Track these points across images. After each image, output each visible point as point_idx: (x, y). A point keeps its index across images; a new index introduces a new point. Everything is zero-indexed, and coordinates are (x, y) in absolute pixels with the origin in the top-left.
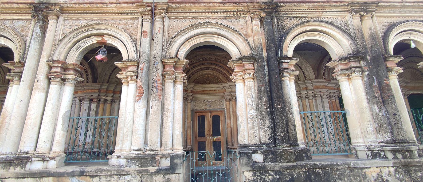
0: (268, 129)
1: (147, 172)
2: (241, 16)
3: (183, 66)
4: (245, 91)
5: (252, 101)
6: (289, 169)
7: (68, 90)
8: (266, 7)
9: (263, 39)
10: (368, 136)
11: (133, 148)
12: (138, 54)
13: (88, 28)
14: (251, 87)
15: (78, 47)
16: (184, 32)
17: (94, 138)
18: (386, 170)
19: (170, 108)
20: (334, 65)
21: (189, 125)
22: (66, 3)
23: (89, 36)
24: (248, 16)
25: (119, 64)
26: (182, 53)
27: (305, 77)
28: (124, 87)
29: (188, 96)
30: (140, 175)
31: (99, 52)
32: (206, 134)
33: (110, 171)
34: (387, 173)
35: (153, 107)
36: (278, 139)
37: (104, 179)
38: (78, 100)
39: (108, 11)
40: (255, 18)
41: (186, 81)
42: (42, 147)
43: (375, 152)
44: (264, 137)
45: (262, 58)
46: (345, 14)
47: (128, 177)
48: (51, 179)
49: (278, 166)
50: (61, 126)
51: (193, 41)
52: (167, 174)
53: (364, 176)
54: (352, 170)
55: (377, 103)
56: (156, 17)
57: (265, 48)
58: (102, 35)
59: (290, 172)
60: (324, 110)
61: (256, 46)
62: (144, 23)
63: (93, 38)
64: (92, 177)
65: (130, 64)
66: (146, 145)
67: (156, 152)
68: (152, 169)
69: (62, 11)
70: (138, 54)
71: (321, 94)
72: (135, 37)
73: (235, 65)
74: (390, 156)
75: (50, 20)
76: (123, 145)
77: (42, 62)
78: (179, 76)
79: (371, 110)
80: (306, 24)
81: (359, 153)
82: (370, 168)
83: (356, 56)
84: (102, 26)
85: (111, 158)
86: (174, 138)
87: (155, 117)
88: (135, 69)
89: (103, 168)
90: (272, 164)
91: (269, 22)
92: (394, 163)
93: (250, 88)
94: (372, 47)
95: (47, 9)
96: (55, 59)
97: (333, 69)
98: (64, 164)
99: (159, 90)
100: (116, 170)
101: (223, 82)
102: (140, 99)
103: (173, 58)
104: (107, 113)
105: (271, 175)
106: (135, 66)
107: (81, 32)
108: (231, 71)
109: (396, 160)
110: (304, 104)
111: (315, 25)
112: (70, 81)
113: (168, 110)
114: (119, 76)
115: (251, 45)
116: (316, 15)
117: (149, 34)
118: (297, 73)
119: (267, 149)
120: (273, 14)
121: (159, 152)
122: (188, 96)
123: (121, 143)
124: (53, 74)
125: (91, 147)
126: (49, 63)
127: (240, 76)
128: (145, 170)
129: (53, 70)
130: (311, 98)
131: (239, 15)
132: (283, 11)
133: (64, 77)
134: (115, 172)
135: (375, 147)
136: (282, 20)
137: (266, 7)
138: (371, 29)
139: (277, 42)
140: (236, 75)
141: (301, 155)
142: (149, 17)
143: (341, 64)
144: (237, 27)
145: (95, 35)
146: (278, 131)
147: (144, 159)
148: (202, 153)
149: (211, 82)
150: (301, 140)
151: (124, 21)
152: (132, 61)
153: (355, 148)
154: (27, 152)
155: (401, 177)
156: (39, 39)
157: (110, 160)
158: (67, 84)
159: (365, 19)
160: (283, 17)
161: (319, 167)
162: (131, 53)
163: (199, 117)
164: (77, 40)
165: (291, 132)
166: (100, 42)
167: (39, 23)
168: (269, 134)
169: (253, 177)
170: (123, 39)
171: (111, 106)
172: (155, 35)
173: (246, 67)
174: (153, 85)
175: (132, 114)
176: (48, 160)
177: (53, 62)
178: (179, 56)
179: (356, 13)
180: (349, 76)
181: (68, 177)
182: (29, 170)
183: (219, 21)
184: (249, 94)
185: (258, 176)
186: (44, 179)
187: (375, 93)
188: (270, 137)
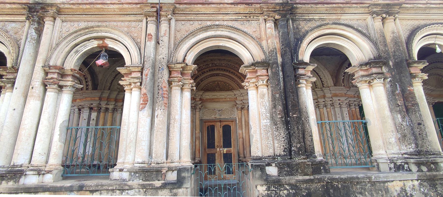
0: (283, 139)
1: (152, 187)
3: (191, 71)
4: (259, 99)
5: (265, 109)
6: (306, 183)
7: (66, 98)
10: (390, 147)
11: (136, 160)
12: (143, 59)
13: (87, 30)
14: (265, 94)
15: (77, 52)
16: (193, 35)
17: (94, 150)
18: (410, 184)
19: (177, 117)
21: (198, 135)
23: (88, 40)
24: (261, 18)
25: (121, 70)
26: (190, 58)
27: (323, 84)
28: (127, 95)
29: (196, 105)
30: (144, 190)
31: (100, 57)
32: (216, 146)
33: (112, 186)
34: (411, 186)
36: (294, 150)
38: (77, 108)
39: (109, 12)
42: (38, 160)
43: (398, 164)
44: (279, 149)
45: (277, 63)
46: (366, 17)
49: (293, 179)
50: (59, 136)
51: (202, 45)
52: (174, 189)
53: (387, 191)
54: (373, 184)
55: (400, 112)
57: (280, 53)
58: (102, 38)
60: (343, 119)
62: (148, 25)
63: (93, 42)
67: (162, 164)
68: (158, 184)
69: (59, 12)
70: (143, 59)
72: (139, 40)
73: (247, 71)
74: (414, 168)
75: (46, 22)
76: (125, 157)
78: (187, 82)
79: (394, 119)
80: (323, 27)
81: (381, 166)
82: (392, 181)
83: (378, 61)
84: (103, 29)
85: (113, 171)
86: (181, 150)
88: (139, 75)
90: (287, 178)
91: (284, 24)
92: (419, 176)
93: (264, 95)
95: (43, 11)
96: (51, 64)
97: (353, 75)
98: (61, 178)
99: (165, 97)
100: (119, 185)
101: (234, 89)
103: (180, 63)
104: (109, 122)
106: (139, 71)
107: (80, 34)
108: (243, 77)
109: (420, 173)
111: (334, 28)
112: (68, 88)
114: (121, 83)
115: (264, 49)
116: (334, 17)
117: (154, 37)
118: (314, 79)
119: (282, 162)
120: (288, 16)
121: (165, 165)
123: (123, 155)
126: (45, 68)
127: (253, 83)
128: (149, 185)
129: (50, 76)
130: (329, 107)
131: (252, 17)
132: (299, 13)
133: (61, 83)
135: (398, 159)
138: (393, 33)
139: (292, 46)
140: (248, 82)
141: (319, 168)
142: (154, 19)
143: (361, 70)
145: (96, 38)
146: (294, 142)
148: (211, 166)
150: (319, 152)
151: (127, 23)
153: (376, 160)
154: (21, 165)
155: (426, 191)
156: (34, 42)
157: (111, 174)
159: (387, 21)
160: (299, 20)
161: (337, 180)
162: (134, 57)
163: (208, 127)
164: (75, 44)
166: (100, 45)
168: (284, 145)
169: (266, 192)
172: (161, 39)
173: (259, 74)
174: (158, 93)
175: (135, 124)
176: (44, 174)
177: (50, 67)
178: (187, 62)
179: (378, 15)
180: (369, 82)
182: (23, 184)
183: (230, 24)
184: (262, 102)
185: (272, 190)
187: (399, 101)
188: (285, 148)
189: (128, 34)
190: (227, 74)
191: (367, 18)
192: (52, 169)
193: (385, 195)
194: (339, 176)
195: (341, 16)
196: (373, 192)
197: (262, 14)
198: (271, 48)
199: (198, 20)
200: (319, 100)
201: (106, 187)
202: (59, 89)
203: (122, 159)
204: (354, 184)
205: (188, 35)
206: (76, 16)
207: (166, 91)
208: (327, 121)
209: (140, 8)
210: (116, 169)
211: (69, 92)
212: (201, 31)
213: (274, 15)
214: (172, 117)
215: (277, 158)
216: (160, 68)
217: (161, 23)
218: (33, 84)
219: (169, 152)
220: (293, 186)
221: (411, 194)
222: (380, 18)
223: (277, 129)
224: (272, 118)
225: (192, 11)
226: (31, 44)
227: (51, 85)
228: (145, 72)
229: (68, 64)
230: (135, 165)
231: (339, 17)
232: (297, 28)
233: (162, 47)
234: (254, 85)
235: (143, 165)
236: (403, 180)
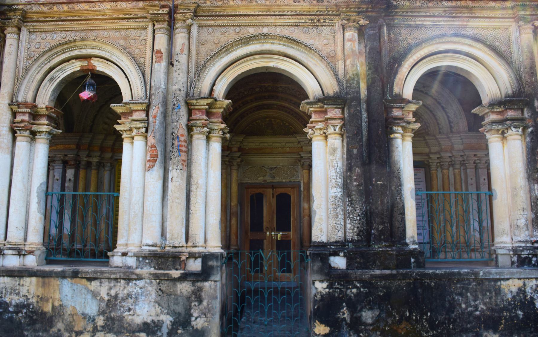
0: (358, 218)
1: (168, 277)
2: (325, 22)
3: (222, 110)
4: (327, 155)
5: (336, 172)
6: (385, 280)
7: (42, 149)
8: (368, 7)
10: (517, 232)
11: (145, 241)
12: (148, 90)
15: (52, 79)
16: (225, 51)
20: (483, 113)
21: (234, 209)
22: (30, 4)
23: (67, 60)
24: (337, 23)
25: (117, 108)
26: (221, 89)
27: (451, 127)
29: (232, 158)
30: (158, 281)
31: (85, 86)
32: (264, 227)
33: (114, 273)
35: (174, 180)
36: (374, 234)
37: (107, 283)
39: (97, 15)
40: (350, 27)
42: (15, 236)
43: (523, 256)
44: (351, 231)
46: (508, 24)
47: (141, 283)
48: (34, 279)
49: (367, 274)
50: (37, 205)
51: (240, 66)
52: (198, 281)
53: (498, 291)
54: (480, 282)
56: (177, 26)
57: (365, 80)
59: (385, 283)
60: (478, 188)
61: (348, 77)
62: (156, 36)
63: (73, 63)
64: (90, 280)
65: (135, 108)
66: (164, 238)
67: (180, 249)
68: (176, 274)
70: (148, 90)
72: (142, 60)
73: (311, 109)
75: (8, 36)
76: (128, 236)
78: (216, 127)
80: (438, 40)
81: (500, 258)
82: (508, 279)
84: (89, 43)
85: (113, 256)
87: (177, 195)
88: (143, 115)
89: (104, 269)
90: (359, 272)
91: (372, 35)
93: (335, 150)
96: (20, 99)
97: (482, 118)
98: (45, 262)
99: (182, 151)
101: (296, 133)
102: (153, 166)
103: (204, 98)
104: (81, 185)
106: (144, 110)
108: (305, 119)
110: (446, 177)
111: (455, 43)
112: (43, 136)
113: (197, 184)
114: (118, 127)
115: (340, 78)
117: (165, 56)
118: (417, 126)
119: (354, 250)
120: (380, 21)
121: (184, 249)
125: (81, 230)
126: (12, 107)
127: (320, 129)
128: (165, 275)
129: (19, 118)
130: (458, 166)
131: (322, 21)
132: (400, 15)
133: (35, 128)
134: (122, 275)
135: (524, 249)
136: (397, 30)
137: (368, 7)
139: (385, 71)
140: (312, 128)
141: (404, 258)
142: (165, 25)
143: (493, 112)
144: (317, 42)
146: (375, 222)
147: (163, 259)
149: (275, 134)
150: (413, 237)
151: (123, 32)
152: (139, 103)
153: (495, 251)
157: (111, 259)
158: (213, 139)
161: (430, 277)
162: (135, 88)
163: (252, 197)
164: (50, 68)
166: (84, 68)
168: (359, 226)
169: (327, 290)
172: (175, 58)
173: (329, 115)
174: (173, 144)
175: (141, 190)
176: (24, 255)
177: (18, 105)
180: (503, 133)
181: (56, 279)
182: (2, 266)
183: (286, 32)
184: (332, 161)
185: (336, 288)
186: (25, 279)
188: (360, 231)
189: (125, 49)
191: (510, 26)
192: (34, 249)
194: (434, 271)
196: (479, 294)
198: (350, 74)
199: (234, 26)
200: (442, 154)
201: (107, 275)
202: (32, 136)
203: (124, 239)
204: (453, 282)
205: (218, 52)
206: (49, 23)
207: (185, 141)
208: (453, 192)
209: (144, 8)
210: (117, 252)
212: (238, 45)
213: (357, 18)
214: (194, 181)
215: (348, 245)
216: (174, 105)
217: (176, 31)
219: (190, 231)
220: (365, 283)
222: (529, 28)
223: (351, 203)
224: (346, 187)
225: (224, 10)
227: (22, 132)
228: (152, 112)
229: (41, 100)
230: (143, 248)
231: (465, 23)
232: (396, 40)
233: (178, 72)
234: (322, 133)
235: (154, 248)
236: (524, 279)
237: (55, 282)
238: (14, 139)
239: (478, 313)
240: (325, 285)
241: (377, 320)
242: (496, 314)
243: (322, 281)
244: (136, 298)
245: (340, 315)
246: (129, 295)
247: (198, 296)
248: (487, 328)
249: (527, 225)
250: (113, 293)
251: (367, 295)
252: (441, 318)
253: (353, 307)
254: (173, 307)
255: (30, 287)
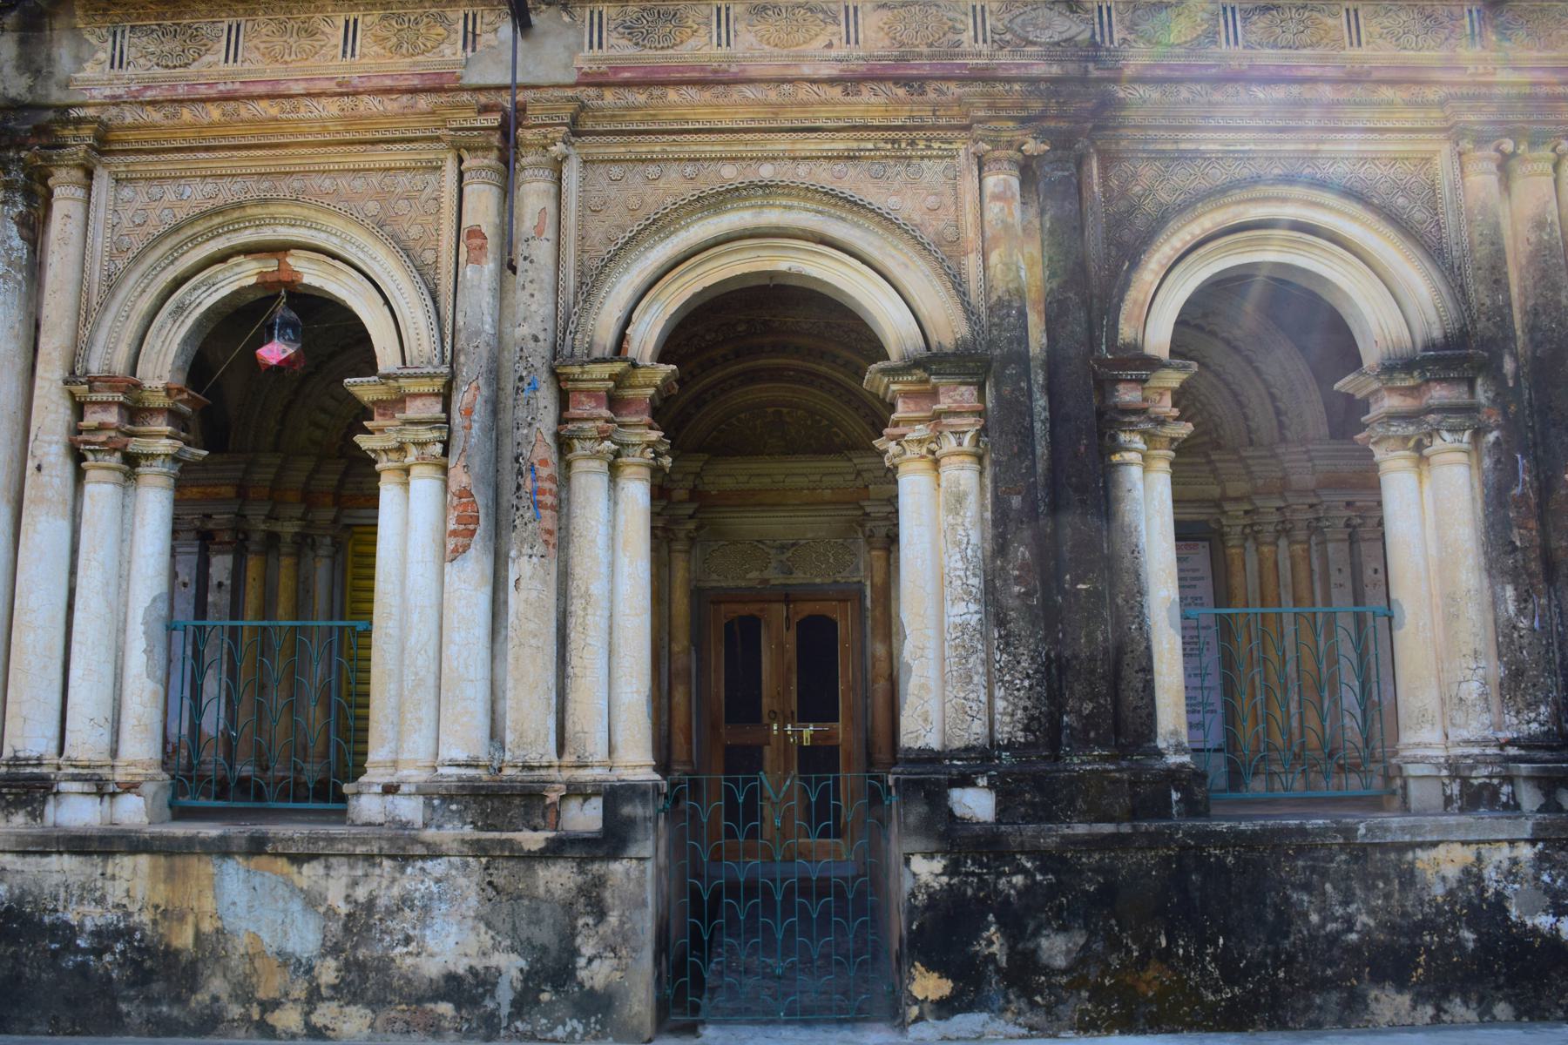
0: (1026, 683)
2: (929, 147)
3: (651, 391)
4: (940, 511)
5: (964, 558)
7: (154, 504)
9: (1031, 266)
10: (1459, 718)
11: (447, 753)
12: (448, 340)
13: (219, 219)
14: (966, 494)
15: (180, 309)
16: (658, 231)
17: (232, 719)
19: (598, 588)
21: (680, 662)
22: (116, 105)
23: (222, 258)
24: (963, 148)
25: (363, 388)
27: (1281, 426)
28: (388, 493)
30: (484, 860)
32: (765, 711)
33: (365, 841)
34: (1506, 864)
35: (523, 584)
36: (1068, 726)
38: (194, 533)
40: (997, 160)
41: (667, 461)
42: (86, 742)
43: (1476, 782)
45: (1023, 359)
47: (437, 867)
48: (143, 861)
51: (699, 270)
52: (593, 859)
53: (1409, 877)
54: (1360, 852)
55: (1514, 576)
56: (524, 161)
59: (1102, 859)
61: (994, 298)
62: (467, 190)
63: (238, 265)
64: (298, 859)
67: (543, 772)
68: (533, 840)
69: (105, 143)
70: (448, 340)
71: (1348, 513)
72: (429, 256)
73: (894, 387)
74: (1530, 798)
75: (57, 192)
76: (399, 738)
77: (47, 384)
78: (635, 439)
79: (1496, 602)
80: (1238, 194)
82: (1434, 844)
83: (1455, 355)
84: (282, 210)
85: (358, 794)
86: (617, 725)
87: (532, 626)
88: (434, 409)
89: (335, 830)
90: (1030, 829)
92: (1538, 827)
93: (960, 499)
94: (1536, 314)
95: (44, 141)
96: (95, 367)
98: (168, 813)
99: (545, 507)
100: (390, 840)
102: (466, 548)
103: (603, 360)
105: (1021, 870)
106: (436, 395)
107: (193, 238)
108: (877, 416)
109: (1547, 817)
110: (1269, 564)
112: (159, 467)
113: (587, 596)
114: (364, 441)
117: (492, 244)
119: (1016, 770)
121: (553, 774)
122: (682, 523)
123: (391, 734)
124: (92, 438)
125: (271, 721)
126: (74, 388)
127: (920, 442)
128: (502, 843)
129: (92, 419)
130: (1301, 535)
131: (922, 144)
132: (1135, 126)
133: (135, 445)
134: (386, 846)
135: (1479, 761)
138: (1540, 225)
140: (898, 439)
141: (1153, 791)
142: (492, 159)
143: (1392, 390)
145: (249, 250)
146: (1072, 694)
147: (496, 801)
148: (736, 781)
149: (792, 449)
150: (1175, 733)
151: (375, 179)
152: (423, 376)
153: (1400, 768)
154: (38, 759)
155: (1559, 882)
156: (19, 277)
157: (352, 802)
159: (1518, 169)
162: (412, 333)
163: (729, 626)
164: (175, 279)
165: (1131, 697)
167: (15, 204)
168: (1028, 704)
169: (945, 879)
170: (377, 268)
171: (297, 564)
172: (521, 249)
173: (945, 403)
174: (519, 487)
175: (432, 614)
176: (113, 795)
177: (91, 382)
178: (631, 354)
179: (1480, 141)
180: (1419, 447)
181: (205, 858)
182: (55, 826)
183: (823, 175)
185: (968, 874)
186: (118, 859)
187: (1515, 531)
188: (1032, 718)
189: (381, 227)
190: (823, 369)
191: (1435, 152)
193: (1397, 896)
195: (1321, 141)
197: (967, 128)
199: (680, 160)
200: (1258, 503)
202: (127, 468)
203: (387, 748)
204: (1286, 855)
205: (639, 232)
207: (551, 478)
209: (433, 113)
210: (370, 784)
211: (162, 481)
212: (693, 212)
213: (1018, 136)
214: (576, 587)
215: (999, 757)
216: (521, 379)
218: (38, 453)
219: (569, 725)
220: (1046, 859)
221: (1498, 893)
222: (1490, 159)
223: (1007, 642)
224: (991, 597)
226: (11, 284)
227: (100, 456)
228: (461, 399)
231: (1313, 147)
233: (530, 288)
234: (924, 451)
235: (471, 772)
236: (1478, 842)
237: (203, 867)
238: (79, 476)
239: (1353, 937)
240: (938, 865)
241: (1082, 958)
242: (1404, 941)
243: (929, 855)
244: (426, 908)
245: (980, 947)
246: (406, 901)
247: (593, 900)
248: (1378, 978)
249: (1484, 696)
250: (361, 894)
251: (1052, 891)
252: (1253, 951)
253: (1014, 928)
254: (525, 931)
255: (132, 883)
